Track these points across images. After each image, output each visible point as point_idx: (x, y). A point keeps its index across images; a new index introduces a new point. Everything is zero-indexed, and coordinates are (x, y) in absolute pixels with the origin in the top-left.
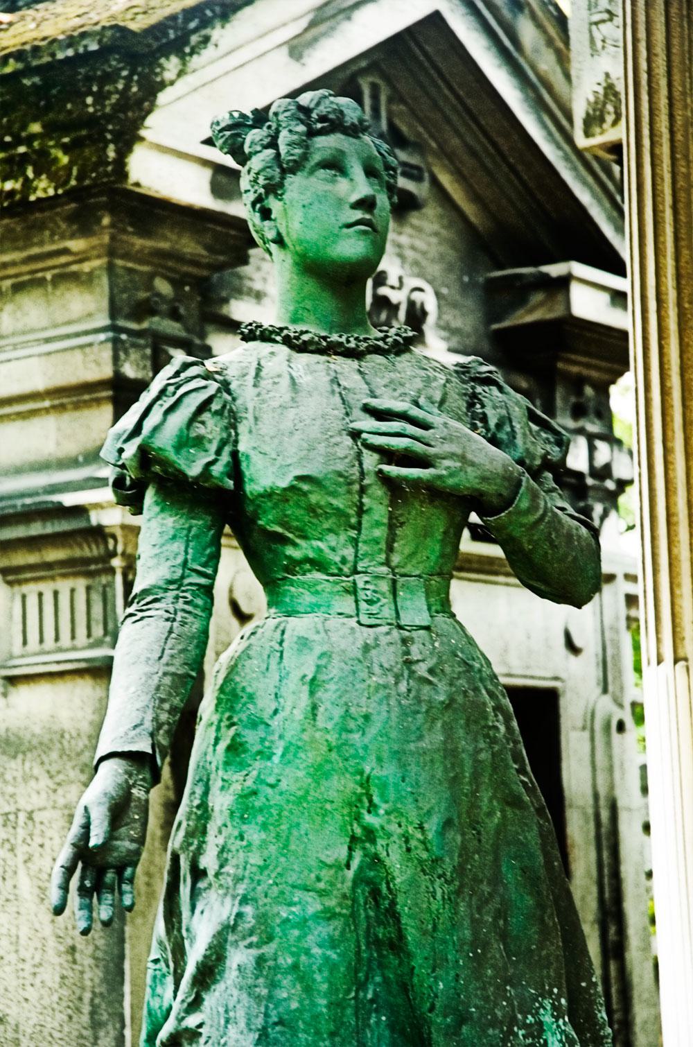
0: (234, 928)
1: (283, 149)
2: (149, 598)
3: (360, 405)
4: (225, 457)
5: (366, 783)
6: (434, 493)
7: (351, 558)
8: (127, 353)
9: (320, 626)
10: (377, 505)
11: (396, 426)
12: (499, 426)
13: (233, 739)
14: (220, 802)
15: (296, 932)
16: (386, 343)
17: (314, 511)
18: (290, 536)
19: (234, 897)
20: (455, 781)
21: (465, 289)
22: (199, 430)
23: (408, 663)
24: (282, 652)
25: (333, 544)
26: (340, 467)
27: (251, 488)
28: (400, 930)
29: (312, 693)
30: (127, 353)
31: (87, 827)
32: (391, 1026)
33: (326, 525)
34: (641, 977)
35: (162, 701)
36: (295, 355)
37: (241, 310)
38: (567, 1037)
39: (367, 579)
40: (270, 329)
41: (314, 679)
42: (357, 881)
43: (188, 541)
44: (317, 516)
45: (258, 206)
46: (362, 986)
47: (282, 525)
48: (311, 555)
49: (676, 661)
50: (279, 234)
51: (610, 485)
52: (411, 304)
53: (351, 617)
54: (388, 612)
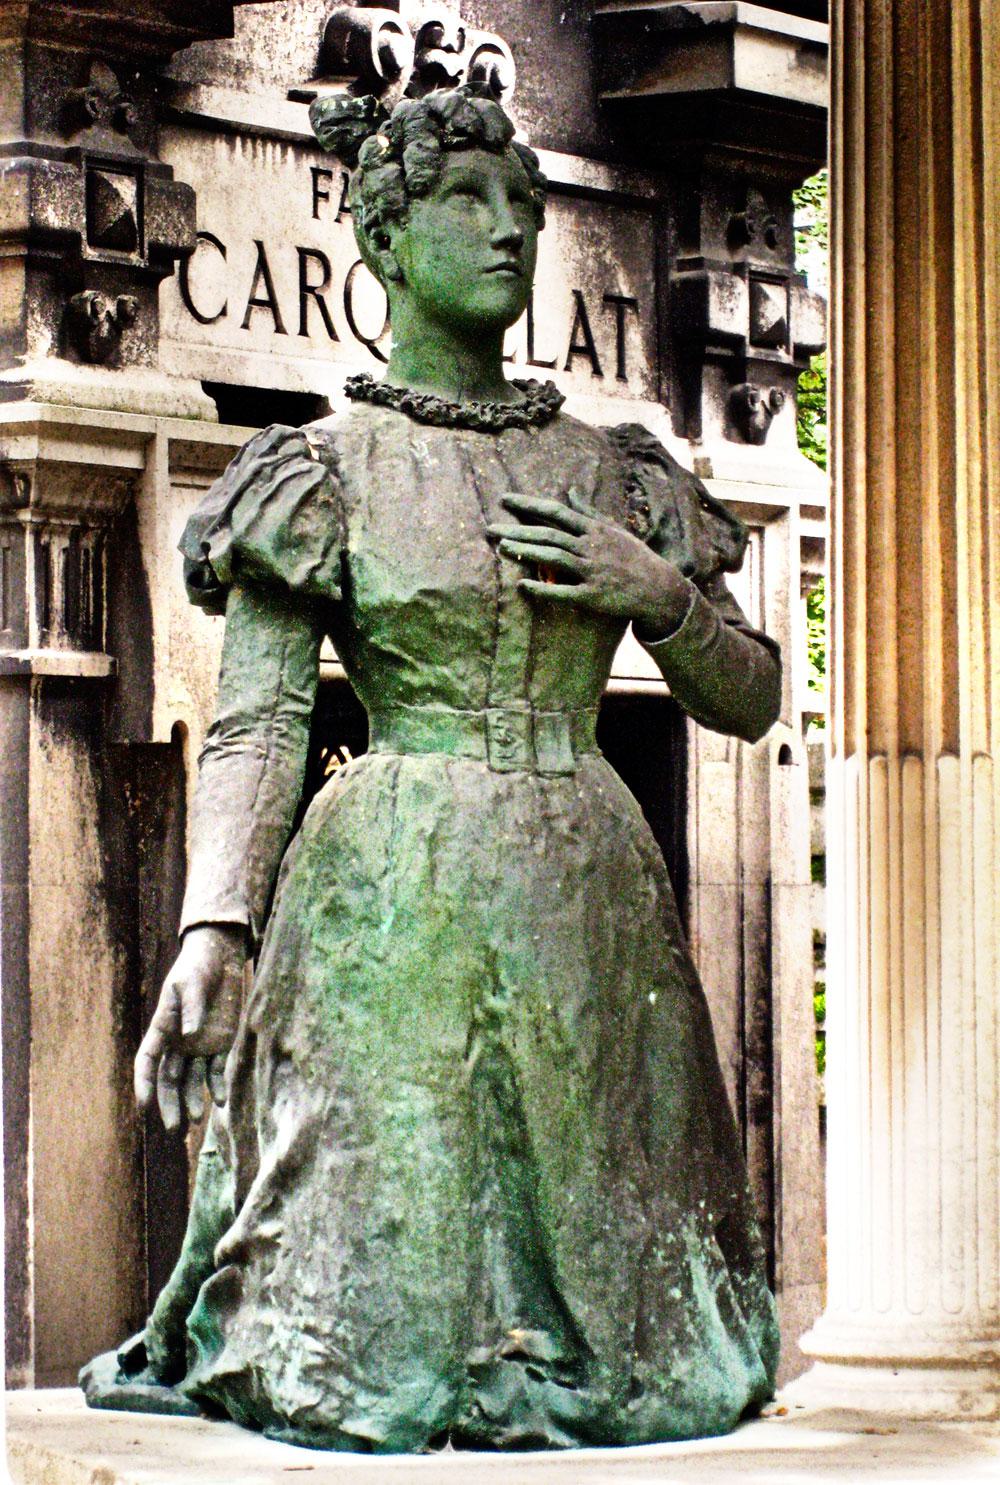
0: (326, 1124)
1: (410, 168)
2: (237, 729)
3: (498, 500)
4: (333, 560)
5: (492, 959)
6: (583, 612)
7: (483, 689)
8: (48, 185)
9: (442, 770)
10: (517, 628)
11: (542, 532)
12: (663, 521)
13: (332, 901)
14: (316, 975)
15: (402, 1133)
16: (527, 412)
17: (440, 632)
18: (410, 658)
19: (328, 1089)
20: (593, 961)
21: (561, 32)
22: (306, 526)
23: (547, 819)
24: (395, 800)
25: (461, 671)
26: (475, 581)
27: (361, 599)
28: (524, 1132)
29: (431, 851)
30: (48, 185)
31: (178, 1009)
32: (508, 1242)
33: (454, 649)
34: (797, 1151)
35: (257, 860)
36: (417, 428)
37: (216, 101)
38: (714, 1260)
39: (501, 714)
40: (386, 390)
41: (433, 836)
42: (477, 1073)
43: (283, 660)
44: (443, 637)
45: (373, 231)
46: (476, 1196)
47: (404, 646)
48: (434, 682)
49: (870, 754)
50: (400, 269)
51: (784, 356)
52: (477, 73)
53: (480, 759)
54: (522, 755)
